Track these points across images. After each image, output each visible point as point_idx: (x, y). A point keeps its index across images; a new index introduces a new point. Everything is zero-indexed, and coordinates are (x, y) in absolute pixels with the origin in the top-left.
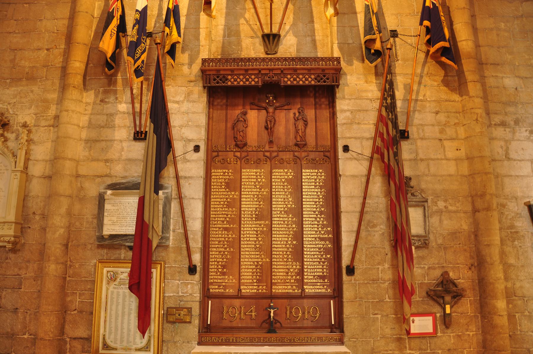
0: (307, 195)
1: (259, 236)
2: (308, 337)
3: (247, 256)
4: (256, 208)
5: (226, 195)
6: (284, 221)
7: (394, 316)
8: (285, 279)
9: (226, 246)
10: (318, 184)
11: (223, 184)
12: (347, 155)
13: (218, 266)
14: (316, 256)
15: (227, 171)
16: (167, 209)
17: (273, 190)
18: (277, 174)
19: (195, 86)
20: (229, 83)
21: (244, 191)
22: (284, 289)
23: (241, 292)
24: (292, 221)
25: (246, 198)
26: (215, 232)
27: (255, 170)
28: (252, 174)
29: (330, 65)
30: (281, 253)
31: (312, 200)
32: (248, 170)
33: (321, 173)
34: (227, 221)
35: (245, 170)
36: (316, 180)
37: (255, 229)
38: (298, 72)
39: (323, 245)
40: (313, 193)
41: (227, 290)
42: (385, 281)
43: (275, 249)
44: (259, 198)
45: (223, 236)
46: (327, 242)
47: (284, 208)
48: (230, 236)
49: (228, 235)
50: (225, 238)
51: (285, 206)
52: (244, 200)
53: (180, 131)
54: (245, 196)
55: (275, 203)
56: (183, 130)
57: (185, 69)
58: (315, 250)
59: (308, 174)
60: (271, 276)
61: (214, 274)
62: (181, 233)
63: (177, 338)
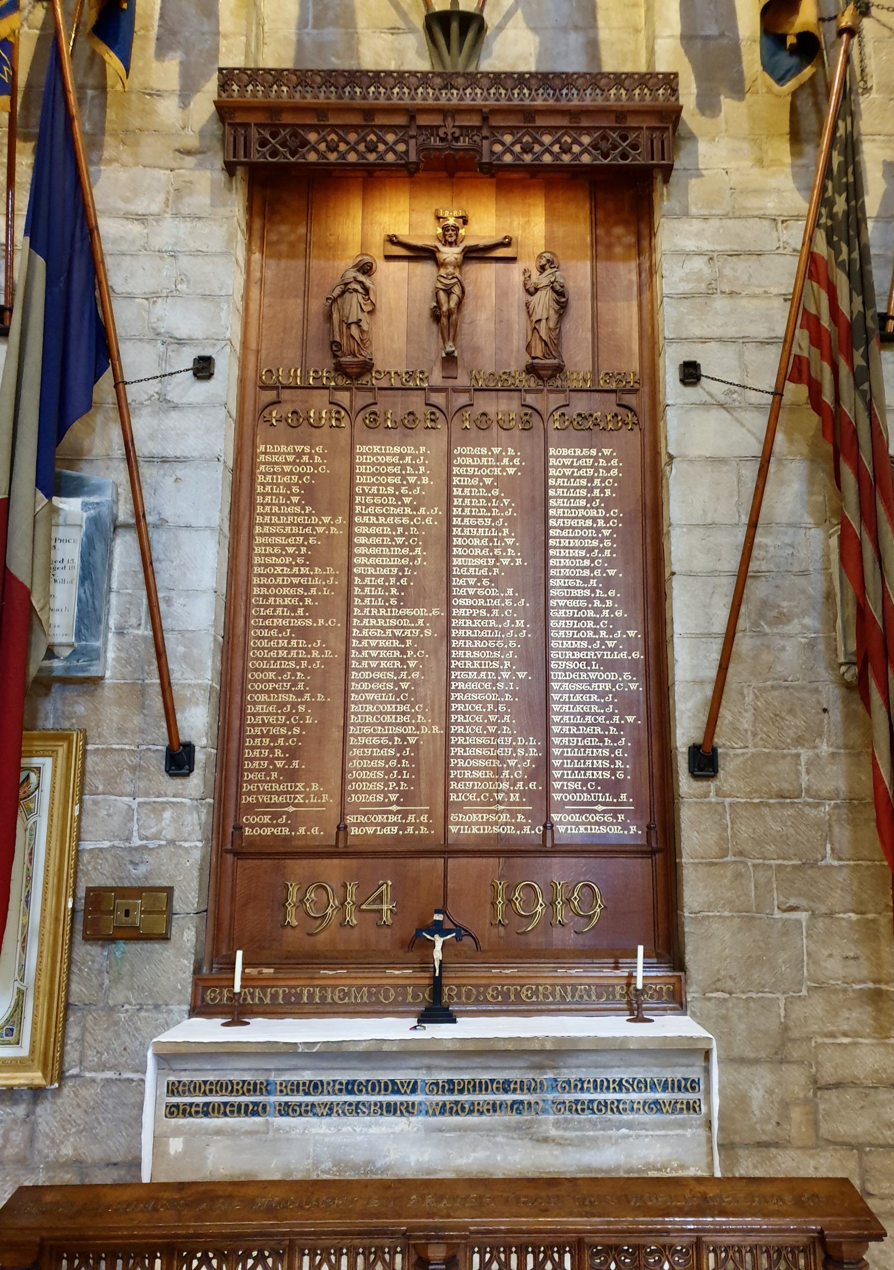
0: (562, 529)
1: (410, 653)
2: (564, 986)
3: (369, 719)
4: (401, 568)
5: (305, 526)
6: (489, 610)
7: (853, 916)
8: (491, 792)
9: (301, 686)
10: (597, 492)
11: (295, 489)
12: (692, 393)
13: (272, 750)
14: (589, 719)
15: (307, 449)
16: (98, 556)
17: (455, 511)
18: (469, 461)
19: (200, 165)
20: (312, 157)
21: (361, 514)
22: (488, 823)
23: (347, 834)
24: (515, 610)
25: (369, 536)
26: (265, 643)
27: (397, 450)
28: (388, 459)
29: (641, 97)
30: (477, 707)
31: (577, 543)
32: (376, 449)
33: (608, 459)
34: (307, 608)
35: (365, 449)
36: (591, 479)
37: (398, 633)
38: (540, 122)
39: (614, 683)
40: (581, 523)
41: (302, 830)
42: (819, 799)
43: (460, 696)
44: (410, 536)
45: (293, 654)
46: (627, 676)
47: (490, 569)
48: (315, 654)
49: (308, 651)
50: (298, 661)
51: (492, 562)
52: (363, 540)
53: (149, 312)
54: (365, 530)
55: (460, 551)
56: (161, 308)
57: (168, 109)
58: (586, 698)
59: (568, 462)
60: (447, 779)
61: (261, 776)
62: (145, 638)
63: (118, 996)
